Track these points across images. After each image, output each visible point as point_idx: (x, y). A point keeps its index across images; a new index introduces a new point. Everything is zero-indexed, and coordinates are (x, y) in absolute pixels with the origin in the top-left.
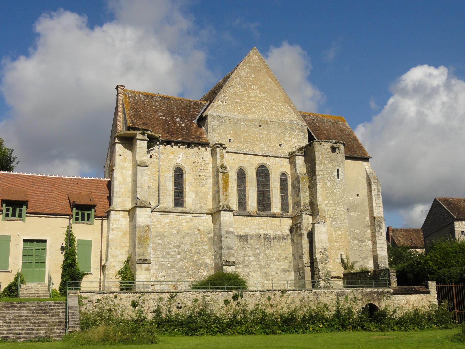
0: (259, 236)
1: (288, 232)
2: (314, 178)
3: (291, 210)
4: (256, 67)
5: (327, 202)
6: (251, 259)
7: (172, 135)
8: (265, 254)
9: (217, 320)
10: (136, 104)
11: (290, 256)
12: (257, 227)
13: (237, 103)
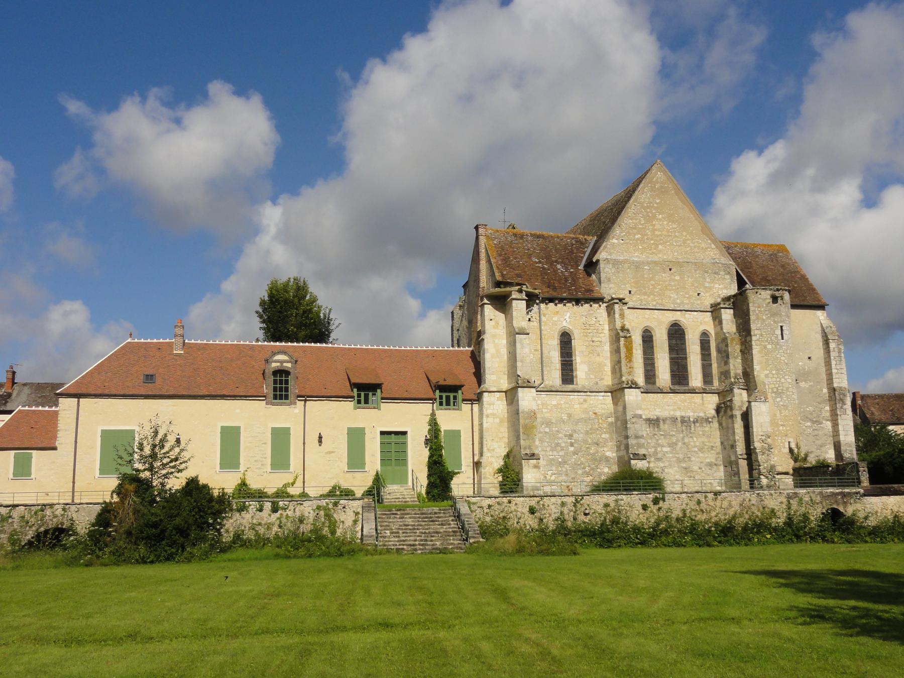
0: (674, 420)
1: (713, 412)
2: (748, 339)
3: (716, 383)
4: (662, 187)
6: (665, 449)
7: (555, 289)
8: (684, 444)
9: (637, 530)
10: (502, 248)
12: (671, 408)
13: (638, 239)
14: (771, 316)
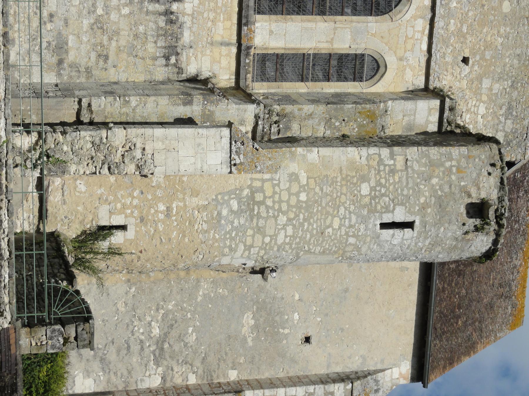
1: (191, 70)
5: (304, 181)
11: (112, 71)
14: (439, 199)
